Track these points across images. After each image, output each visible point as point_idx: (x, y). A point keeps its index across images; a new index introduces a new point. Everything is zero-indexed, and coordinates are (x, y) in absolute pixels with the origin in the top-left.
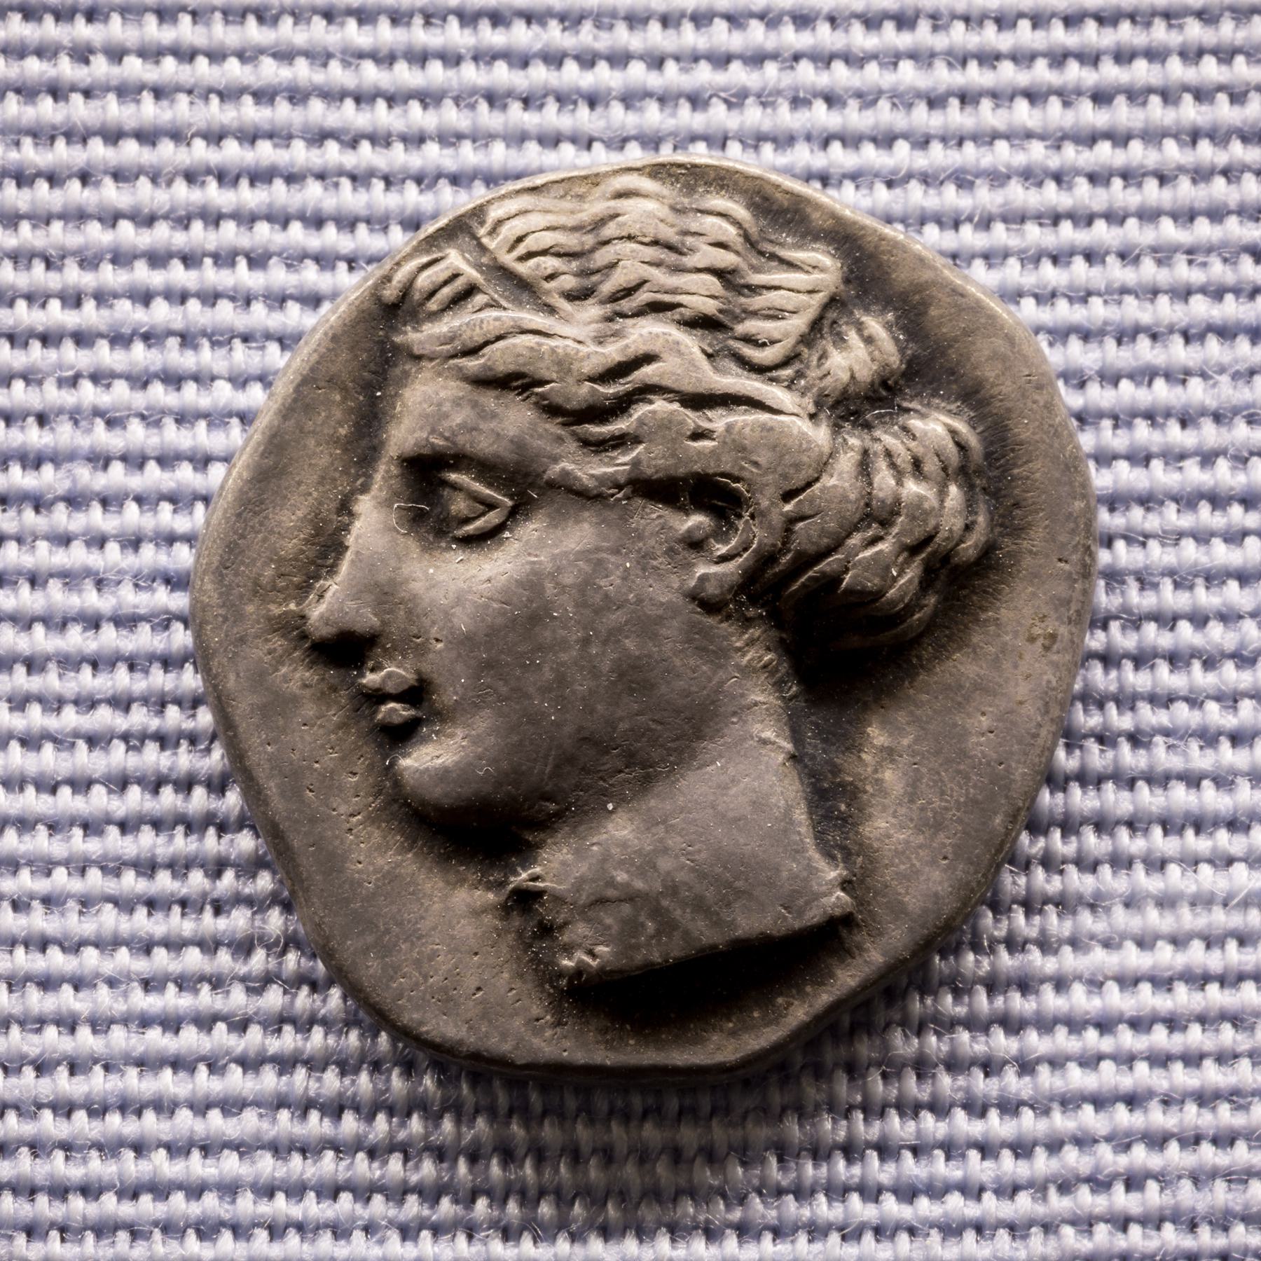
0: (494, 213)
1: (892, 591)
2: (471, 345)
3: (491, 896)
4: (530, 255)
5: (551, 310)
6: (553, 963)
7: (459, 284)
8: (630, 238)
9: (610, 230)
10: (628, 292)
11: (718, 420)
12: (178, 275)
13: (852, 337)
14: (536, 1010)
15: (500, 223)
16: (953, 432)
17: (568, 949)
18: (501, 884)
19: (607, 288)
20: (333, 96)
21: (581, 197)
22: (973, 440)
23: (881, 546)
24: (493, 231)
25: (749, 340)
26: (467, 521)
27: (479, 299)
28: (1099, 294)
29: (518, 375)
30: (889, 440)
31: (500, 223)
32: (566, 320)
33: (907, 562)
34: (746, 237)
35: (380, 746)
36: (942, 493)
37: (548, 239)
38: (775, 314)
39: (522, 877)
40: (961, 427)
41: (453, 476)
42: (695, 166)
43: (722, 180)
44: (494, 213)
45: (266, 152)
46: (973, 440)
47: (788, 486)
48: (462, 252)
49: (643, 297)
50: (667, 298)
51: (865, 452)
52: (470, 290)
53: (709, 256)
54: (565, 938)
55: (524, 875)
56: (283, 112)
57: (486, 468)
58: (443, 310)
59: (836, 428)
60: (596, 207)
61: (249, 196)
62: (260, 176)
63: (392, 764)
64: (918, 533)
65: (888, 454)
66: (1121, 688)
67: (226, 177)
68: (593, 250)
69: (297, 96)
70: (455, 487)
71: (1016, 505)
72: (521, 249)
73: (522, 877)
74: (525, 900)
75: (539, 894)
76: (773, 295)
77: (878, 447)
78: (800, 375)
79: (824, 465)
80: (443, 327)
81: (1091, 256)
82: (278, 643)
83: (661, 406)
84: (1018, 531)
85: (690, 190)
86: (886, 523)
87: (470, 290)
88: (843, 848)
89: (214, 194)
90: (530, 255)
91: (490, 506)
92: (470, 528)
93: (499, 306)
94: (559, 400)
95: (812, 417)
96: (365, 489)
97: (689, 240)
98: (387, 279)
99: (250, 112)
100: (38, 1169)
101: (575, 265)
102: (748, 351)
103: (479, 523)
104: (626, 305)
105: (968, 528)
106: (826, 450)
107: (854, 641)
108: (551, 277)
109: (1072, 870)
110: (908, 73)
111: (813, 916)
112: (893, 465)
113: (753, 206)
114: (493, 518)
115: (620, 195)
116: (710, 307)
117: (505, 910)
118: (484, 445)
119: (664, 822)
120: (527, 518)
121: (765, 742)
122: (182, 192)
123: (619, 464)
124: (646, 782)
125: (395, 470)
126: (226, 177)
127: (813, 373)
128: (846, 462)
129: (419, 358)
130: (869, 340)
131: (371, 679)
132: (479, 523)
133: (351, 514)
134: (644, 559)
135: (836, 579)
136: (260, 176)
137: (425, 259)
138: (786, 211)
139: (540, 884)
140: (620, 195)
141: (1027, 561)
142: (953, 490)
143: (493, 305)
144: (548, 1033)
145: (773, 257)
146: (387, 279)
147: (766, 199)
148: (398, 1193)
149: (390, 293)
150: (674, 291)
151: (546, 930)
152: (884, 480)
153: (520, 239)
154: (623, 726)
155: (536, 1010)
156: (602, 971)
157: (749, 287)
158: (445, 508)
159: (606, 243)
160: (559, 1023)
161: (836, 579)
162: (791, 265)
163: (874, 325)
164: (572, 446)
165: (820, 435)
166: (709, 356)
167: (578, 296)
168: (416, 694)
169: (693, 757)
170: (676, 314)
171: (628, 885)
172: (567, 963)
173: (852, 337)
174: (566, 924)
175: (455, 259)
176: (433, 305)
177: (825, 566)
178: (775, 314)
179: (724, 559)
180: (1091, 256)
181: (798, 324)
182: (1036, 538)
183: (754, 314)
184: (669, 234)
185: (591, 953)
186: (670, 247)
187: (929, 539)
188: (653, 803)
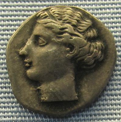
0: (52, 9)
1: (86, 59)
2: (46, 23)
3: (35, 89)
4: (55, 14)
5: (56, 20)
6: (41, 98)
7: (46, 16)
8: (67, 14)
9: (65, 13)
10: (66, 20)
11: (74, 38)
12: (7, 32)
13: (92, 31)
14: (37, 104)
15: (52, 10)
16: (101, 45)
17: (43, 97)
18: (36, 88)
19: (64, 19)
20: (24, 11)
21: (63, 9)
22: (104, 47)
23: (90, 56)
24: (51, 11)
25: (79, 29)
26: (41, 44)
27: (48, 18)
28: (118, 32)
29: (51, 27)
30: (94, 44)
31: (52, 10)
32: (57, 22)
33: (93, 59)
34: (81, 17)
35: (25, 68)
36: (99, 51)
37: (58, 12)
38: (83, 26)
39: (39, 88)
40: (103, 44)
41: (40, 38)
42: (77, 8)
43: (80, 10)
44: (52, 9)
45: (17, 17)
46: (104, 47)
47: (80, 47)
48: (47, 12)
49: (68, 21)
50: (70, 22)
51: (90, 45)
52: (47, 17)
53: (76, 18)
54: (43, 96)
55: (39, 87)
56: (19, 13)
57: (44, 38)
58: (43, 18)
59: (88, 41)
60: (64, 10)
61: (15, 23)
62: (16, 20)
63: (26, 71)
64: (95, 56)
65: (93, 46)
66: (118, 78)
67: (12, 20)
68: (63, 15)
69: (20, 11)
70: (40, 39)
71: (107, 55)
72: (54, 13)
73: (39, 88)
74: (39, 90)
75: (41, 90)
76: (83, 24)
77: (92, 45)
78: (84, 34)
79: (86, 45)
80: (43, 20)
81: (117, 27)
82: (16, 54)
83: (67, 34)
84: (107, 59)
85: (76, 11)
86: (91, 54)
87: (47, 17)
88: (78, 92)
89: (11, 22)
90: (55, 14)
91: (44, 42)
92: (41, 45)
93: (50, 19)
94: (55, 31)
95: (85, 39)
96: (30, 38)
97: (74, 16)
98: (37, 14)
99: (15, 13)
100: (49, 3)
101: (60, 16)
102: (79, 30)
103: (43, 44)
104: (65, 22)
105: (101, 57)
106: (86, 43)
107: (85, 67)
108: (57, 17)
109: (117, 100)
110: (94, 6)
111: (73, 99)
112: (93, 47)
113: (83, 14)
114: (44, 44)
115: (67, 9)
116: (75, 24)
117: (36, 91)
118: (44, 35)
119: (57, 84)
120: (48, 44)
121: (71, 77)
122: (7, 22)
123: (61, 40)
124: (56, 79)
125: (34, 36)
126: (12, 20)
127: (86, 34)
128: (88, 45)
129: (39, 23)
130: (94, 32)
131: (26, 60)
132: (43, 44)
133: (27, 40)
134: (61, 52)
135: (83, 59)
136: (16, 20)
137: (43, 12)
138: (87, 15)
139: (41, 89)
140: (67, 9)
141: (107, 62)
142: (100, 52)
143: (49, 19)
144: (38, 107)
145: (84, 20)
146: (37, 14)
147: (84, 14)
148: (16, 112)
149: (38, 15)
150: (71, 21)
151: (41, 94)
152: (92, 49)
153: (54, 12)
154: (55, 71)
155: (37, 104)
156: (46, 100)
157: (80, 23)
158: (39, 42)
159: (64, 14)
160: (40, 106)
161: (83, 59)
162: (86, 21)
163: (94, 31)
164: (55, 37)
165: (86, 41)
166: (74, 30)
167: (60, 20)
168: (31, 63)
169: (62, 77)
170: (71, 24)
171: (51, 91)
172: (42, 99)
173: (92, 31)
174: (43, 94)
175: (46, 13)
176: (42, 18)
177: (83, 57)
178: (83, 26)
179: (71, 54)
180: (117, 27)
181: (85, 28)
182: (109, 60)
183: (80, 26)
184: (73, 15)
185: (45, 98)
186: (72, 16)
187: (96, 57)
188: (57, 81)
